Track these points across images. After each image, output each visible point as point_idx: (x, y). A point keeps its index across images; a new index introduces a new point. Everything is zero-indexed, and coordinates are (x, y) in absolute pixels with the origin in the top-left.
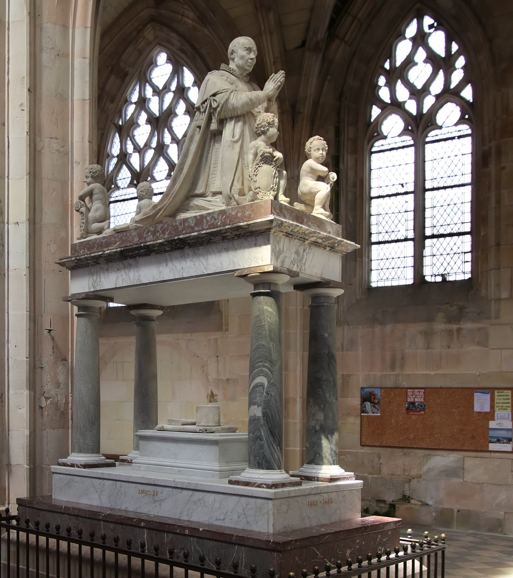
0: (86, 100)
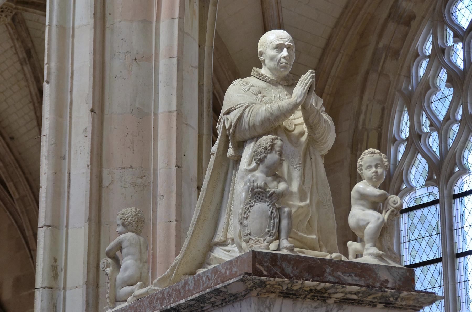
0: (174, 111)
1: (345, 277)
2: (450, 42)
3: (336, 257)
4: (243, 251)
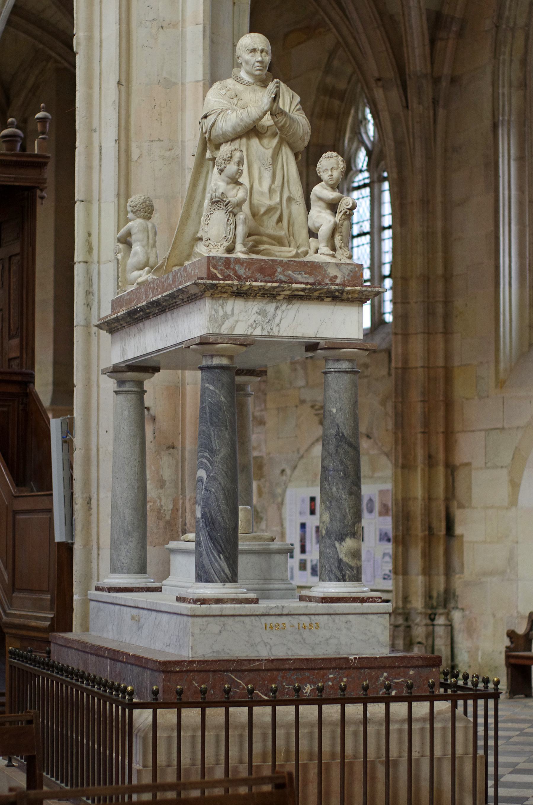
1: (295, 276)
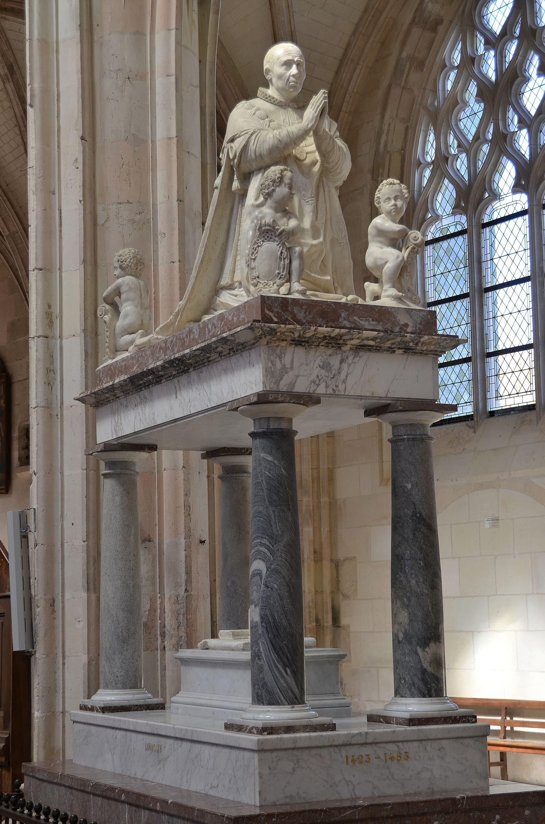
1: (361, 322)
2: (481, 49)
3: (352, 300)
4: (251, 295)
